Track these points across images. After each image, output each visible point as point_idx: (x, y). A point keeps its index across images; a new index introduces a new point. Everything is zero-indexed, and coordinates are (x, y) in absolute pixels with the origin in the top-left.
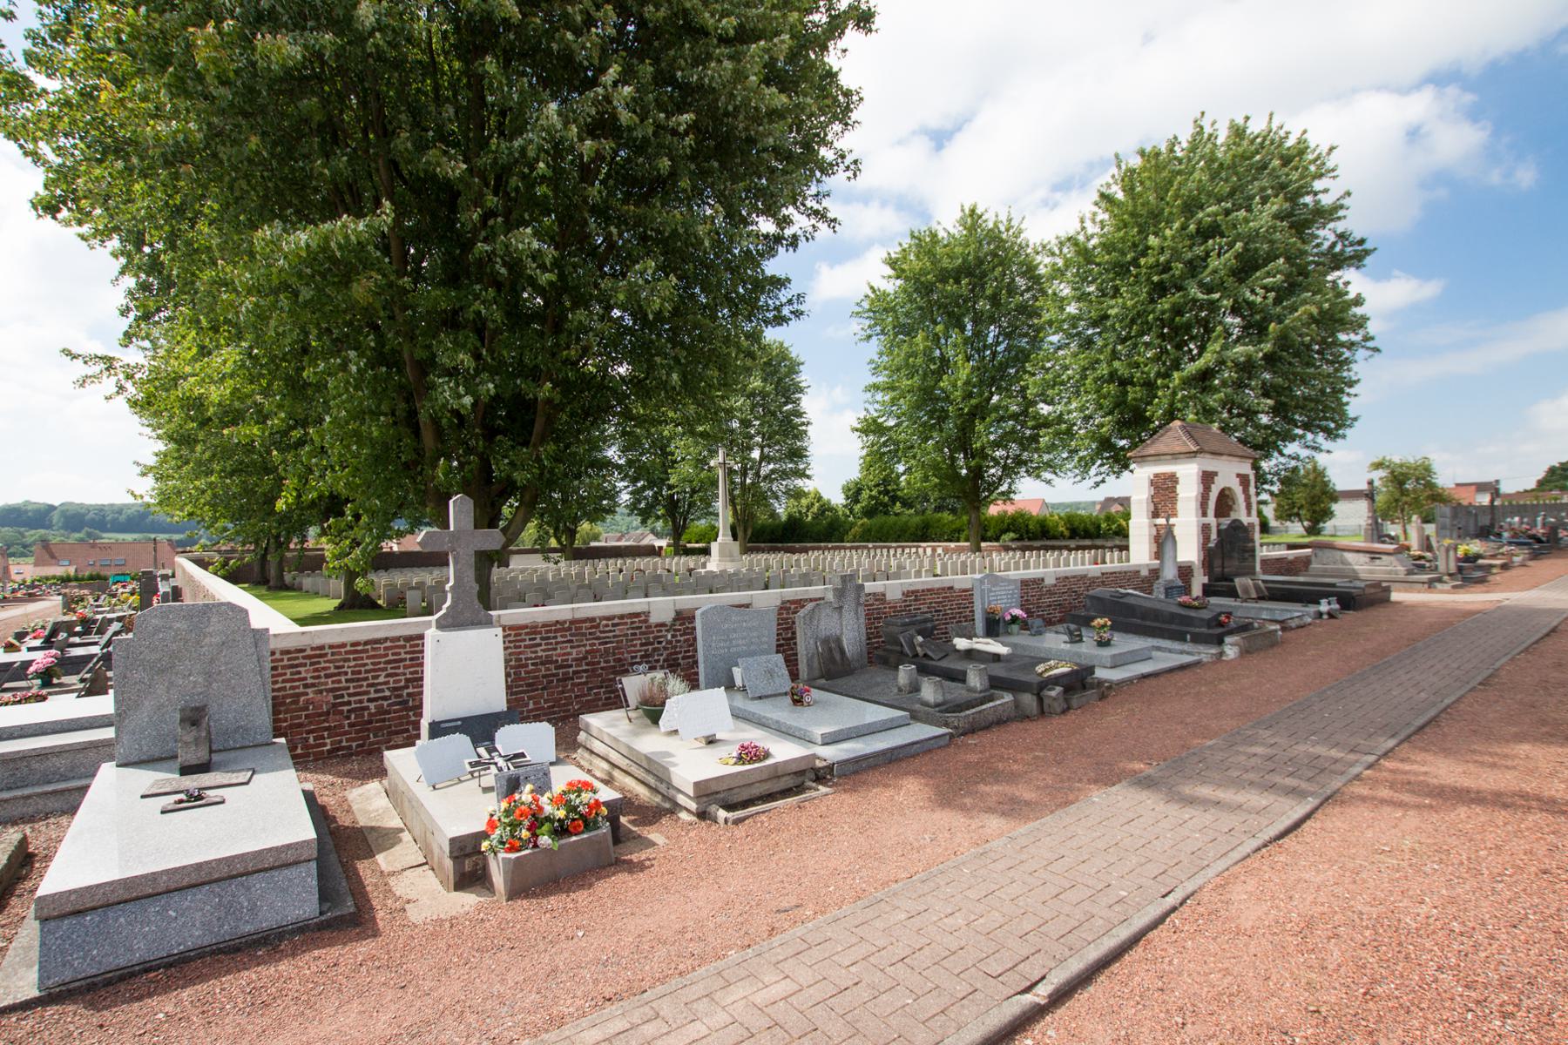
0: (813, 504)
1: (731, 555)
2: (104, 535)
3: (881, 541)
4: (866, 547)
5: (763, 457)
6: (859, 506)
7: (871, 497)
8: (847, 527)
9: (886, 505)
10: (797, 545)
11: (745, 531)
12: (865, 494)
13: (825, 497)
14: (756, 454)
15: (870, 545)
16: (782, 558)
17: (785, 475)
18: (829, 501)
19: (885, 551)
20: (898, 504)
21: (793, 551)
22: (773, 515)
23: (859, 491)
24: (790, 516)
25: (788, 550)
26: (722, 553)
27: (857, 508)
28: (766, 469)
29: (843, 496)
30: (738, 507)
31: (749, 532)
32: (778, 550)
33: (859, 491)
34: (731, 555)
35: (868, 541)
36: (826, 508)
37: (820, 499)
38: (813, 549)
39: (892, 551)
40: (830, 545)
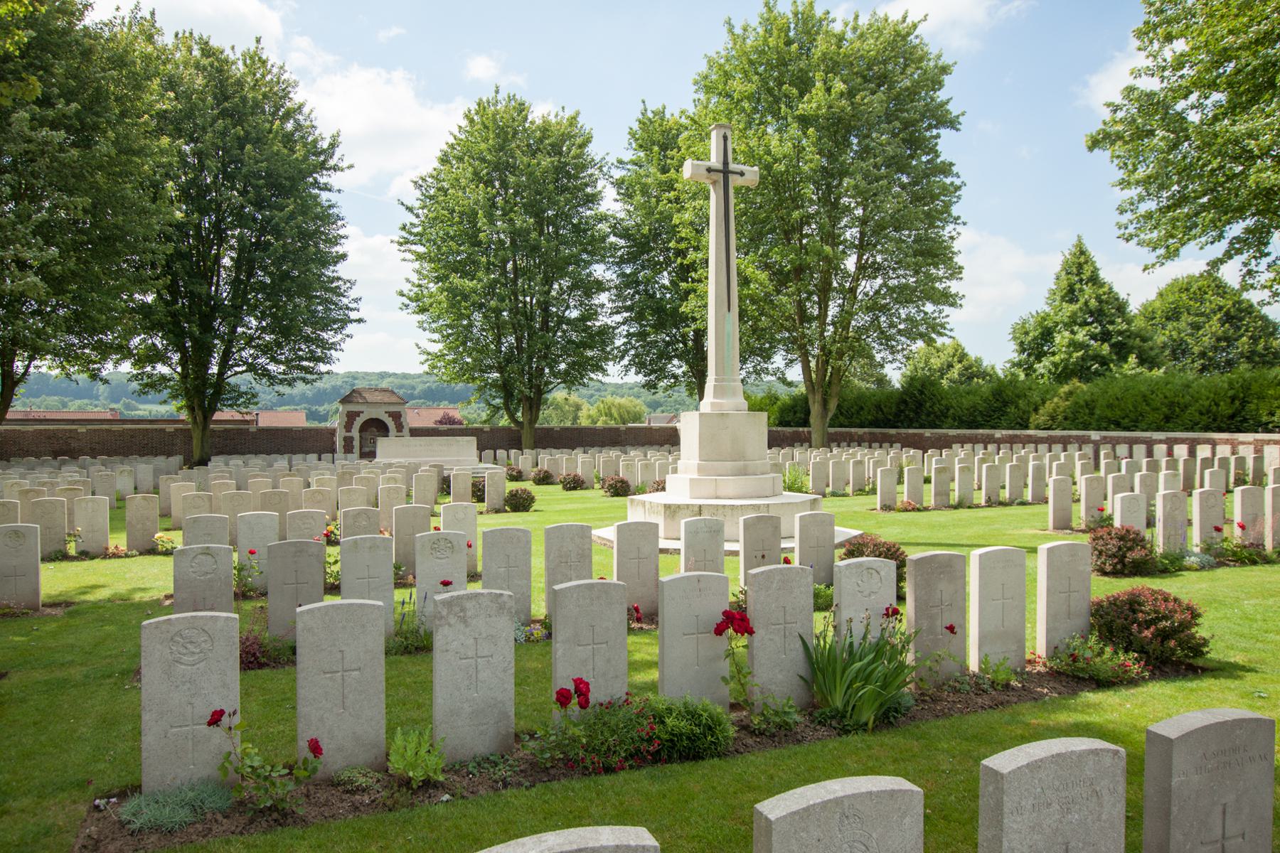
0: (950, 366)
1: (738, 455)
2: (141, 407)
3: (1118, 426)
4: (1082, 441)
5: (861, 267)
6: (1046, 362)
7: (1075, 345)
8: (1036, 398)
9: (1104, 362)
10: (928, 433)
11: (825, 403)
12: (1061, 338)
13: (973, 353)
14: (850, 263)
15: (1095, 435)
16: (897, 459)
17: (904, 295)
18: (978, 361)
19: (1140, 450)
20: (1132, 359)
21: (922, 445)
22: (882, 381)
23: (1047, 334)
24: (911, 381)
25: (908, 443)
26: (711, 453)
27: (1042, 367)
28: (868, 286)
29: (1013, 346)
30: (813, 364)
31: (833, 405)
32: (891, 441)
33: (1047, 334)
34: (738, 455)
35: (1086, 427)
36: (973, 372)
37: (963, 357)
38: (962, 441)
39: (1160, 450)
40: (998, 434)
